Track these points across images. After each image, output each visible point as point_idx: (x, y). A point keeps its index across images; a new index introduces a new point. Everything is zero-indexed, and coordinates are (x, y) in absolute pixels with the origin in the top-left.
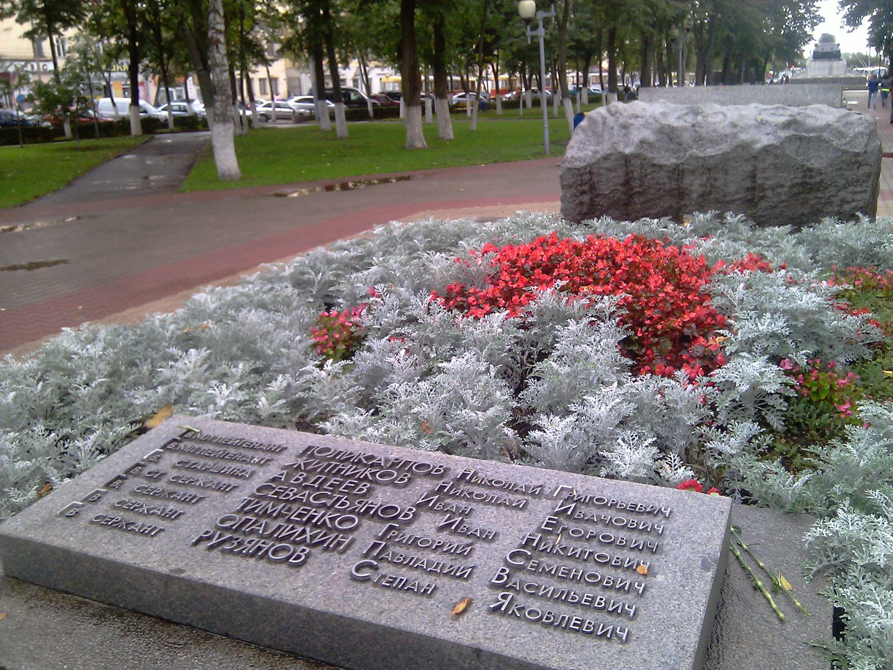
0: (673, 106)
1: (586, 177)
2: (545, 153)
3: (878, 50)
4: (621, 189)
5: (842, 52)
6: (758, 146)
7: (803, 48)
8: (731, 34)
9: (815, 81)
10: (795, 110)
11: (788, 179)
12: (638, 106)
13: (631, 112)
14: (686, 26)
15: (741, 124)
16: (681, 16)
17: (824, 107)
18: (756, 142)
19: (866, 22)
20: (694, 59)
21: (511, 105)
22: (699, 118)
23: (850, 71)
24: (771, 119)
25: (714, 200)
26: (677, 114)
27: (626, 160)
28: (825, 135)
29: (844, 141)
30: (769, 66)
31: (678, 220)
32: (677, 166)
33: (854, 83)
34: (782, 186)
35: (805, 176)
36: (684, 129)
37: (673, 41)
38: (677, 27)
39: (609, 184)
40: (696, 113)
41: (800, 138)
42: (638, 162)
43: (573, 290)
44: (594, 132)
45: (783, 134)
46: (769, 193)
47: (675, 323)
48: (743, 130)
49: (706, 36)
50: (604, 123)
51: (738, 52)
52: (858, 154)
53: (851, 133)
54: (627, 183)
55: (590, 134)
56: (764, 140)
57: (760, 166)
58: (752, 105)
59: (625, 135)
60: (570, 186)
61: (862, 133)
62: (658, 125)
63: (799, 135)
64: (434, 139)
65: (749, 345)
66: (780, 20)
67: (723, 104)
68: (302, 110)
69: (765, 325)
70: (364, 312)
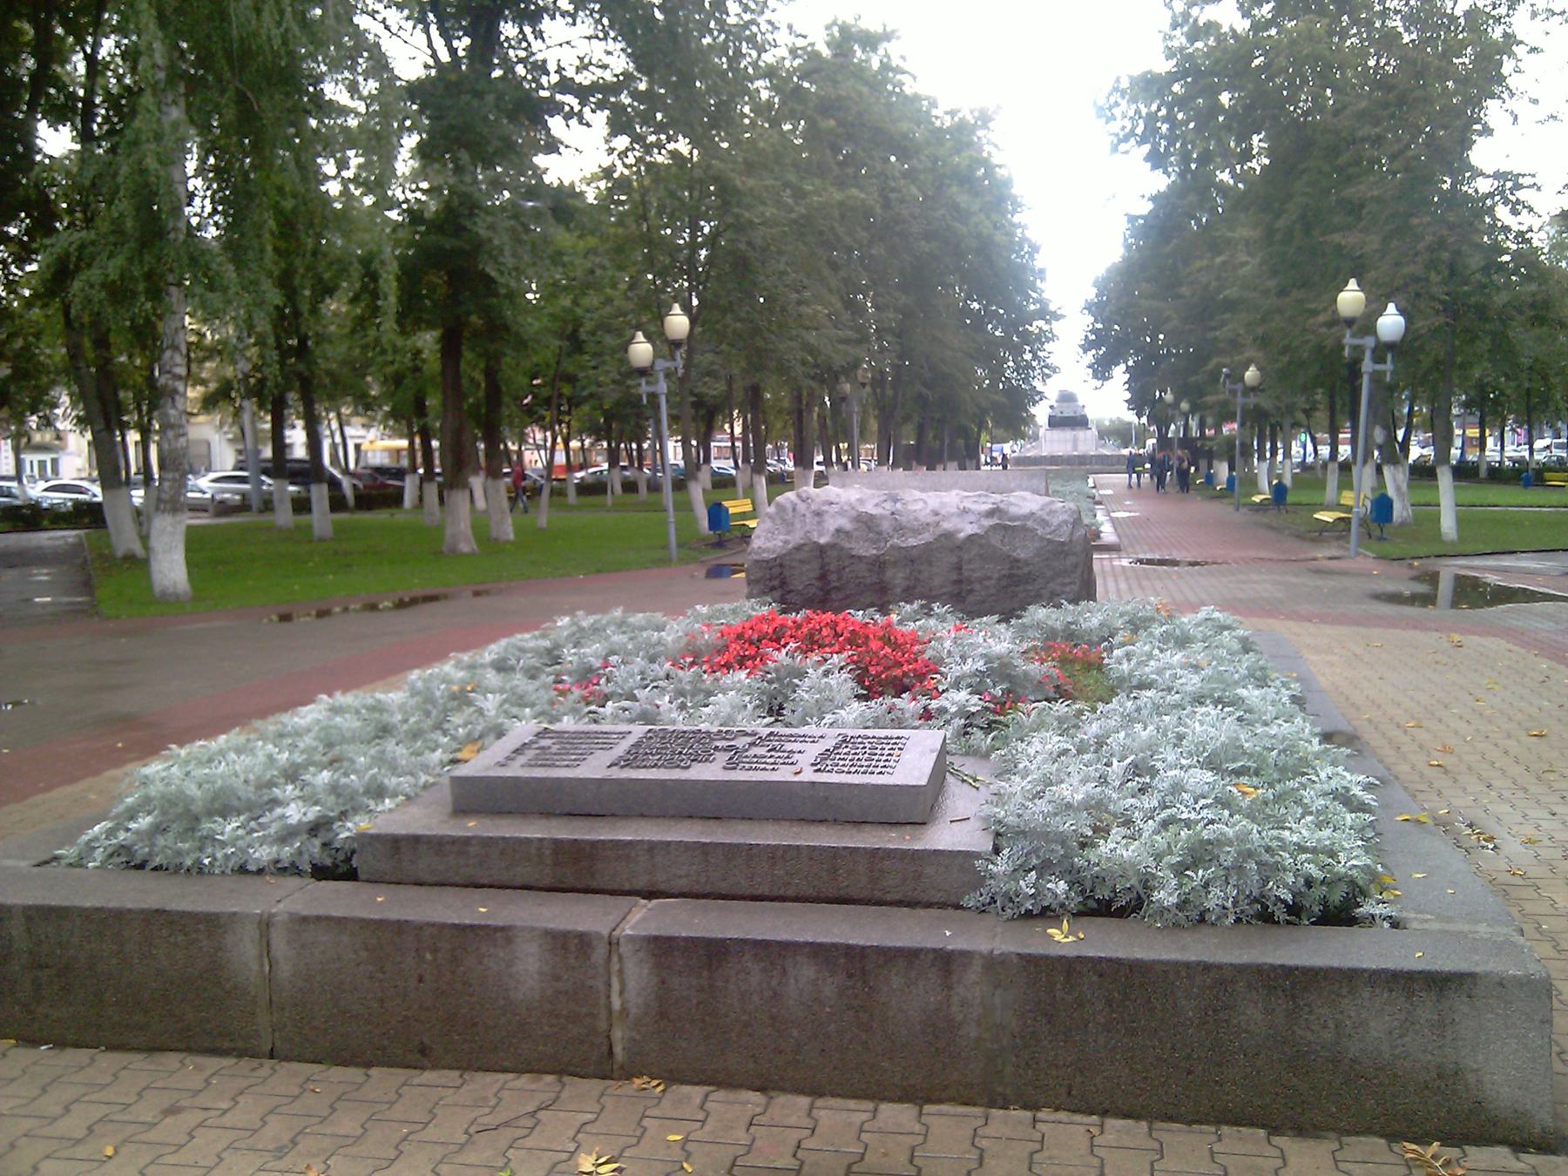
0: (869, 492)
1: (776, 571)
2: (670, 560)
3: (1139, 416)
4: (817, 584)
5: (1090, 417)
6: (962, 535)
7: (1033, 410)
8: (925, 391)
9: (1053, 460)
10: (997, 497)
11: (996, 570)
12: (831, 491)
13: (824, 498)
14: (860, 379)
15: (943, 512)
16: (856, 365)
17: (1027, 494)
18: (959, 531)
19: (1120, 373)
20: (874, 425)
21: (584, 489)
22: (899, 505)
23: (1104, 446)
24: (974, 507)
25: (920, 592)
26: (876, 501)
27: (822, 550)
28: (1029, 523)
29: (1048, 530)
30: (984, 437)
31: (884, 611)
32: (878, 557)
33: (1105, 464)
34: (990, 578)
35: (1012, 568)
36: (882, 517)
37: (843, 399)
38: (847, 380)
39: (804, 578)
40: (896, 501)
41: (1005, 527)
42: (834, 553)
43: (806, 652)
44: (784, 520)
45: (987, 523)
46: (977, 586)
47: (897, 672)
48: (945, 518)
49: (889, 392)
50: (794, 510)
51: (937, 416)
52: (1063, 543)
53: (1055, 522)
54: (823, 577)
55: (778, 521)
56: (968, 529)
57: (966, 557)
58: (954, 492)
59: (819, 523)
60: (757, 581)
61: (1066, 522)
62: (854, 513)
63: (1005, 526)
64: (488, 542)
65: (956, 685)
66: (997, 373)
67: (923, 490)
68: (227, 496)
69: (968, 667)
70: (603, 681)
